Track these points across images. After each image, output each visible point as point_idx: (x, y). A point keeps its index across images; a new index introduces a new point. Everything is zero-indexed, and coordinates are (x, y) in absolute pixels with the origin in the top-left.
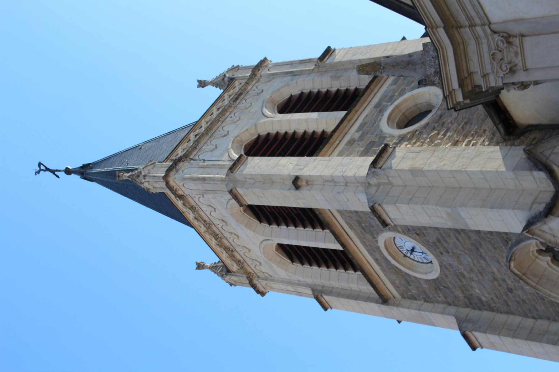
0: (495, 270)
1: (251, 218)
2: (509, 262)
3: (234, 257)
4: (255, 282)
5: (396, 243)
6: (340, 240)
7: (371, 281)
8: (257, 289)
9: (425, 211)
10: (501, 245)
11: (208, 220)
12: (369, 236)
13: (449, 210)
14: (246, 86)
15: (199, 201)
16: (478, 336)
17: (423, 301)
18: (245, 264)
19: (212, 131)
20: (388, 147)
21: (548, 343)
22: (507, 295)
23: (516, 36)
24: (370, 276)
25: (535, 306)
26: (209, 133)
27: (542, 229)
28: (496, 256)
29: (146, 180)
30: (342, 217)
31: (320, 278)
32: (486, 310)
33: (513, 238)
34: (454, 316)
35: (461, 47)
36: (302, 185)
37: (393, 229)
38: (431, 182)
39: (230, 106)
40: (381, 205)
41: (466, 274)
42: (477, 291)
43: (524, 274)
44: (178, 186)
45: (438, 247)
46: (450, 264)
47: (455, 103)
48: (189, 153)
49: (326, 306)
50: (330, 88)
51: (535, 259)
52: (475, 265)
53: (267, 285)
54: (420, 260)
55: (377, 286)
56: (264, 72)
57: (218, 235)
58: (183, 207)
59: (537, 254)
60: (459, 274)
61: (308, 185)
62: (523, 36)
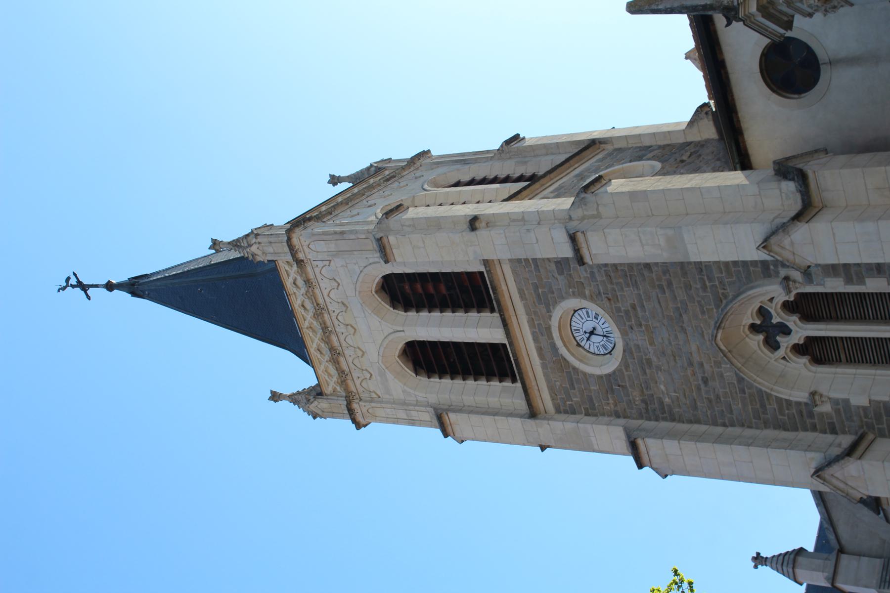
0: (694, 348)
1: (383, 303)
3: (338, 364)
4: (355, 406)
6: (503, 315)
7: (524, 382)
8: (354, 417)
9: (639, 237)
11: (322, 303)
13: (670, 232)
14: (401, 170)
15: (320, 273)
16: (650, 446)
17: (583, 415)
18: (349, 377)
20: (602, 179)
21: (740, 445)
22: (699, 388)
24: (524, 375)
25: (730, 405)
26: (349, 203)
27: (781, 245)
28: (702, 325)
30: (515, 281)
31: (450, 393)
32: (665, 419)
33: (730, 294)
34: (623, 426)
36: (480, 227)
37: (579, 294)
38: (651, 210)
39: (379, 185)
40: (585, 232)
42: (662, 387)
43: (730, 351)
44: (301, 245)
45: (630, 320)
46: (638, 346)
47: (747, 13)
48: (322, 216)
49: (448, 431)
50: (512, 174)
51: (745, 338)
52: (670, 343)
53: (369, 412)
54: (596, 352)
55: (529, 391)
56: (425, 161)
57: (328, 327)
58: (293, 286)
59: (748, 332)
60: (644, 361)
61: (488, 227)
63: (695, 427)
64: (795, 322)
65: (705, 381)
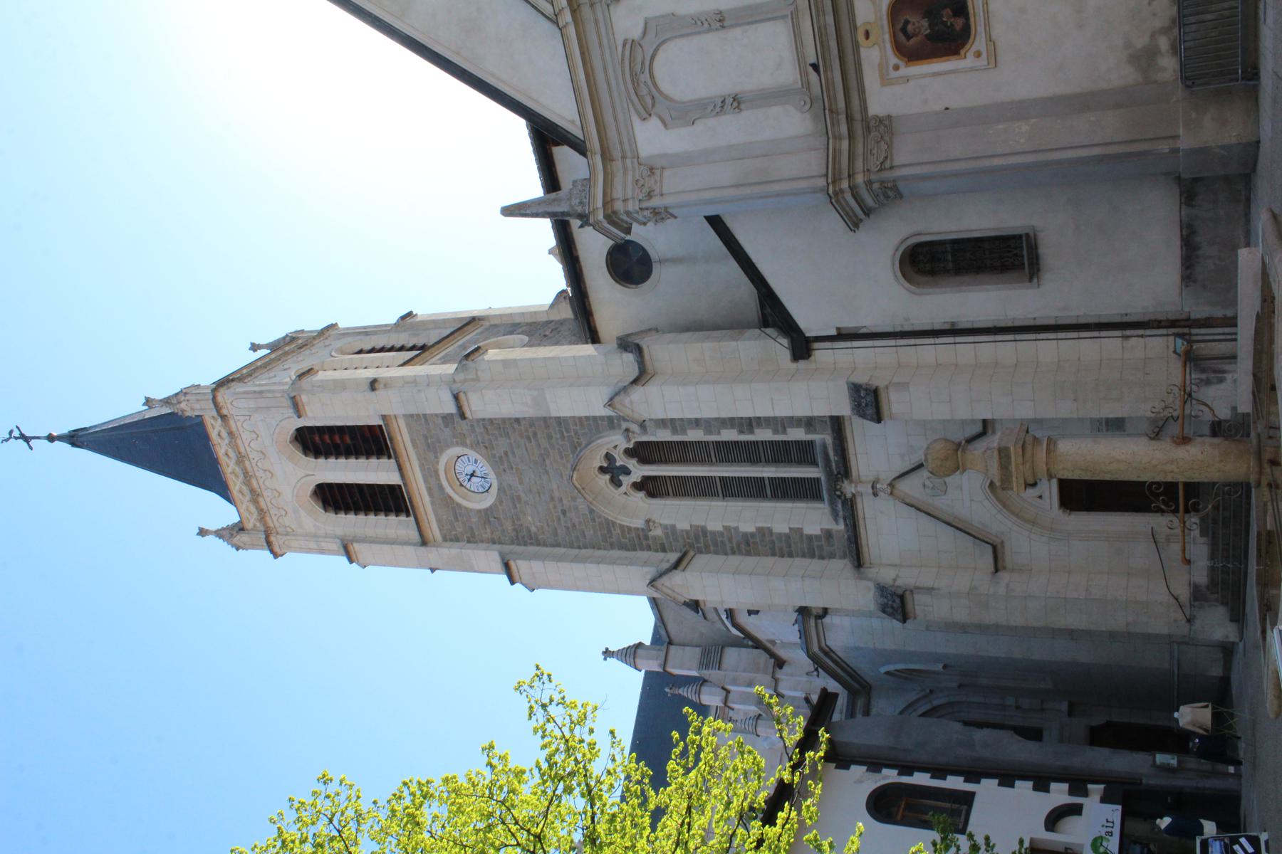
2: (573, 472)
4: (272, 539)
5: (457, 467)
10: (570, 452)
12: (431, 455)
19: (270, 367)
23: (658, 169)
29: (187, 398)
32: (532, 544)
35: (610, 177)
39: (293, 352)
41: (523, 496)
42: (530, 518)
43: (583, 489)
45: (503, 464)
54: (476, 491)
56: (332, 332)
59: (597, 473)
60: (515, 498)
62: (663, 168)
63: (557, 550)
64: (633, 465)
65: (564, 512)
